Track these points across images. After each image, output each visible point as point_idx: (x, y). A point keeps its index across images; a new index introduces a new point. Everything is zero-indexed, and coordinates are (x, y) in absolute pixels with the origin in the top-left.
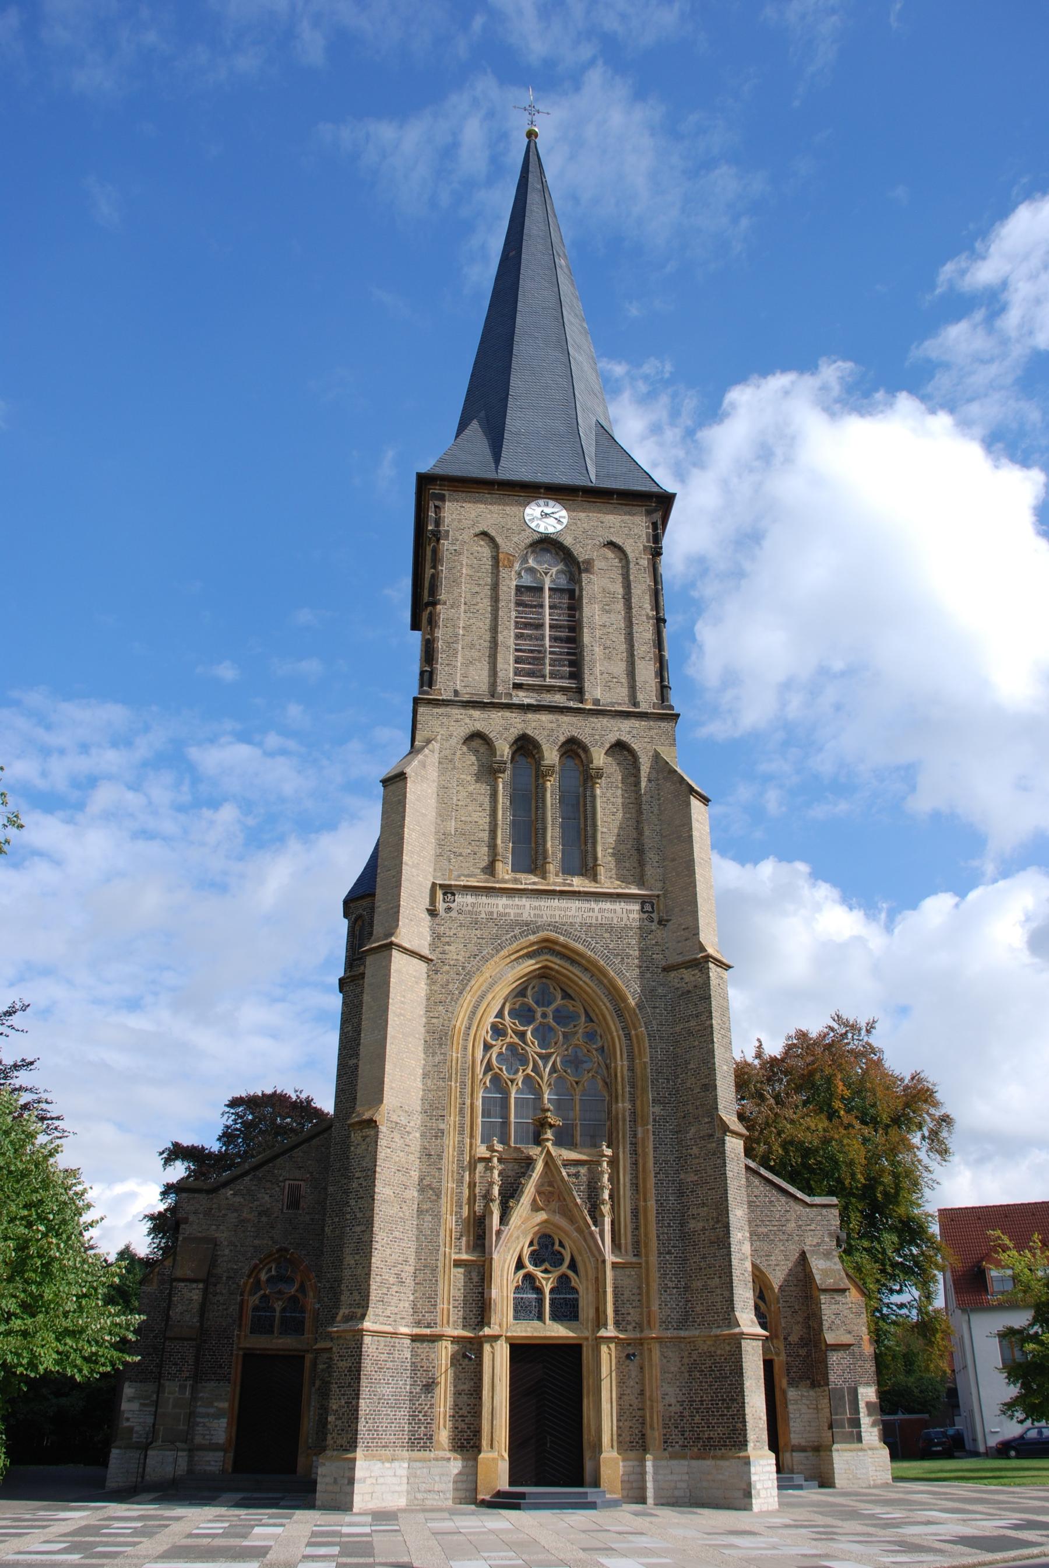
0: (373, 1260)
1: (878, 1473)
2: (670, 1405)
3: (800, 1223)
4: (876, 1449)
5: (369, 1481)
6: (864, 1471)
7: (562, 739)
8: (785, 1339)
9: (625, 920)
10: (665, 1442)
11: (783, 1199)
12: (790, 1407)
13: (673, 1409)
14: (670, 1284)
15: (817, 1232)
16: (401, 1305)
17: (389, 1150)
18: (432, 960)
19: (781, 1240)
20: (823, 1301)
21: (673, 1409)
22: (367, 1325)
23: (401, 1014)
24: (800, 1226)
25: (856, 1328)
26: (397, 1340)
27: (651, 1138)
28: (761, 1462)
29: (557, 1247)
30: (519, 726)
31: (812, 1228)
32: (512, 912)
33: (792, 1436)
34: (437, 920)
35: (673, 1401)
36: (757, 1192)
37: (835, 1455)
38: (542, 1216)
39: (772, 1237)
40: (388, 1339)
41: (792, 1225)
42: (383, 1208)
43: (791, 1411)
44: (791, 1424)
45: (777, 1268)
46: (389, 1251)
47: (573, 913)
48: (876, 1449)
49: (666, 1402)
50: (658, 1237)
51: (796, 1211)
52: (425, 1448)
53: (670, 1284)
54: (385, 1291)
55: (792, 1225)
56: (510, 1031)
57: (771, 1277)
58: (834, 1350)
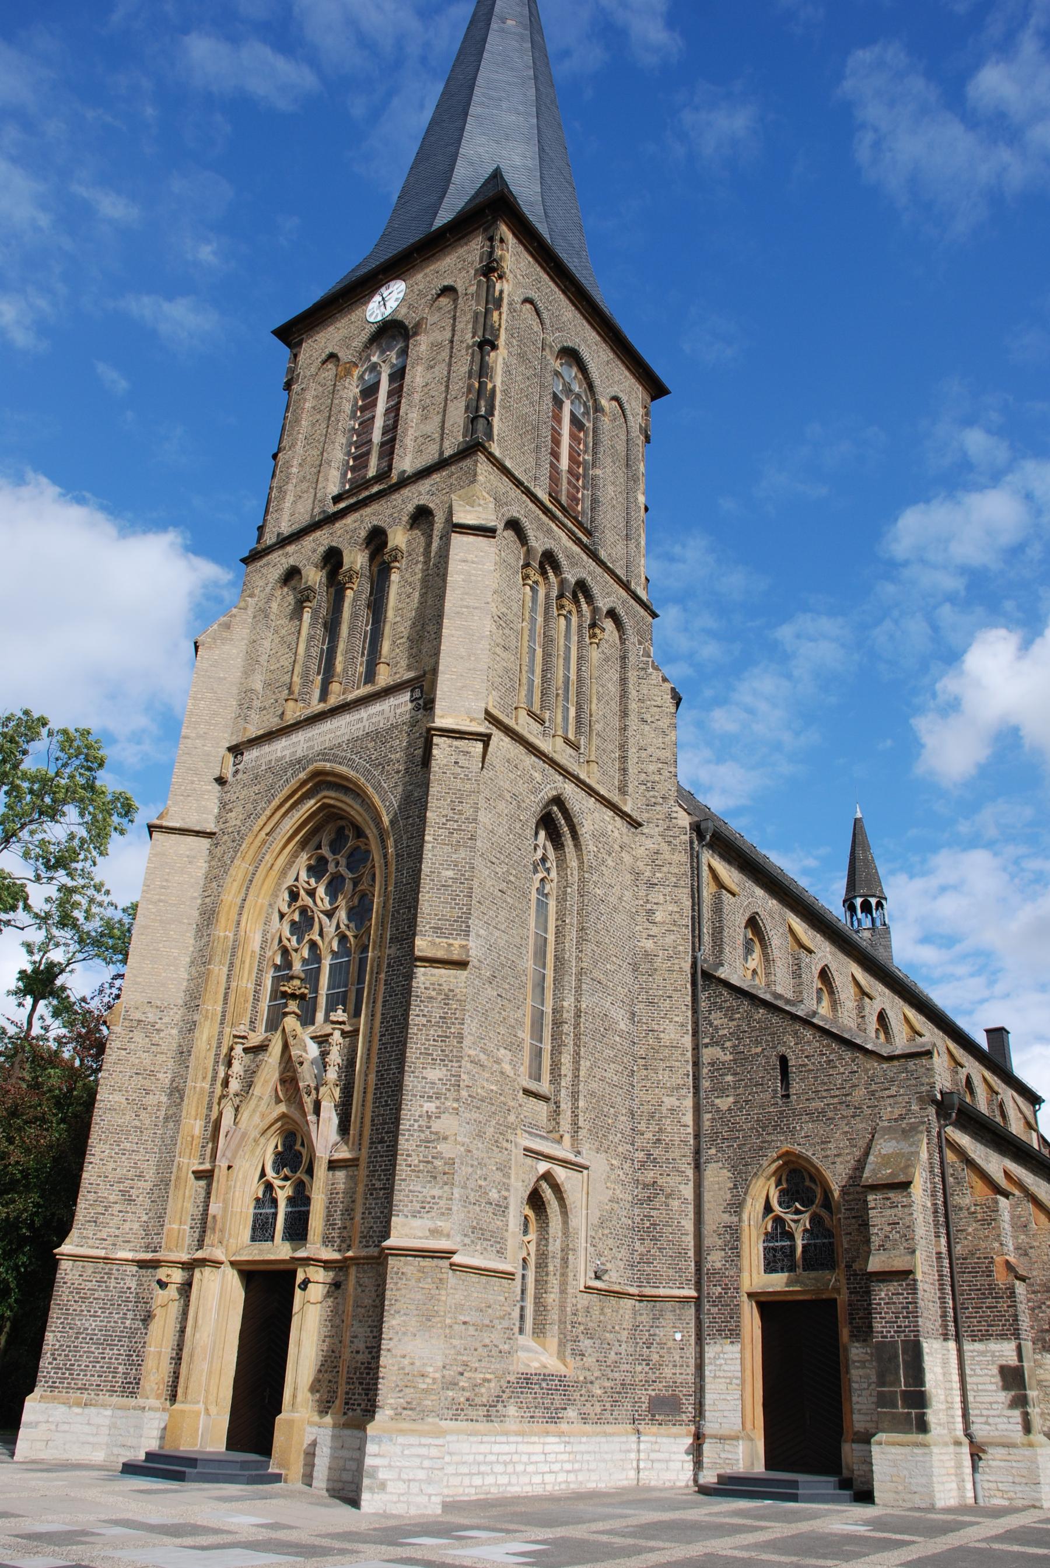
0: (85, 1175)
1: (1018, 1488)
2: (358, 1352)
3: (874, 1087)
4: (1014, 1445)
5: (44, 1427)
6: (923, 1481)
7: (363, 534)
8: (848, 1266)
9: (391, 718)
10: (347, 1403)
11: (848, 1055)
12: (853, 1371)
13: (360, 1357)
14: (378, 1185)
15: (900, 1099)
16: (127, 1226)
17: (124, 1052)
18: (214, 834)
19: (843, 1117)
20: (871, 1205)
21: (360, 1357)
22: (66, 1248)
23: (160, 901)
24: (873, 1093)
25: (983, 1244)
26: (115, 1267)
27: (382, 988)
28: (401, 1440)
29: (298, 1147)
30: (326, 542)
31: (892, 1092)
32: (287, 752)
33: (855, 1417)
34: (227, 788)
35: (362, 1346)
36: (809, 1050)
37: (875, 1449)
38: (282, 1108)
39: (830, 1114)
40: (101, 1265)
41: (860, 1093)
42: (108, 1117)
43: (854, 1378)
44: (855, 1399)
45: (837, 1160)
46: (112, 1165)
47: (343, 731)
48: (1014, 1445)
49: (354, 1347)
50: (373, 1121)
51: (866, 1071)
52: (133, 1394)
53: (378, 1185)
54: (101, 1210)
55: (860, 1093)
56: (302, 892)
57: (828, 1175)
58: (883, 1281)
